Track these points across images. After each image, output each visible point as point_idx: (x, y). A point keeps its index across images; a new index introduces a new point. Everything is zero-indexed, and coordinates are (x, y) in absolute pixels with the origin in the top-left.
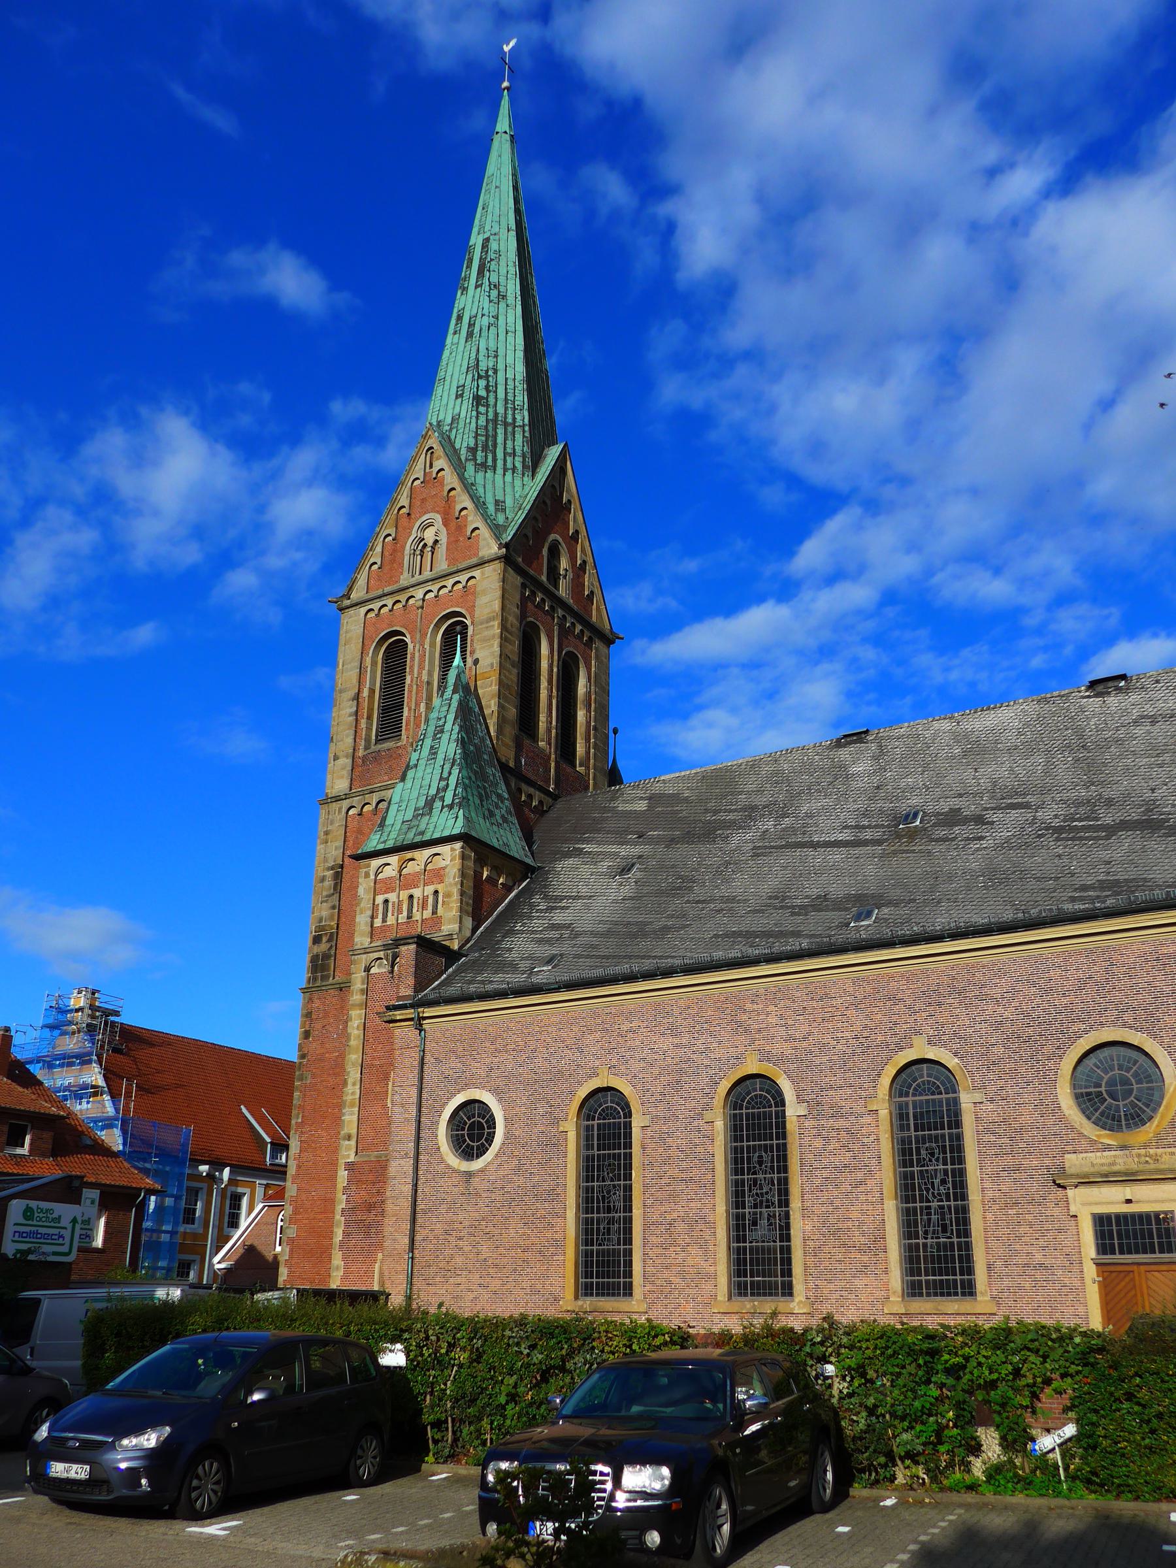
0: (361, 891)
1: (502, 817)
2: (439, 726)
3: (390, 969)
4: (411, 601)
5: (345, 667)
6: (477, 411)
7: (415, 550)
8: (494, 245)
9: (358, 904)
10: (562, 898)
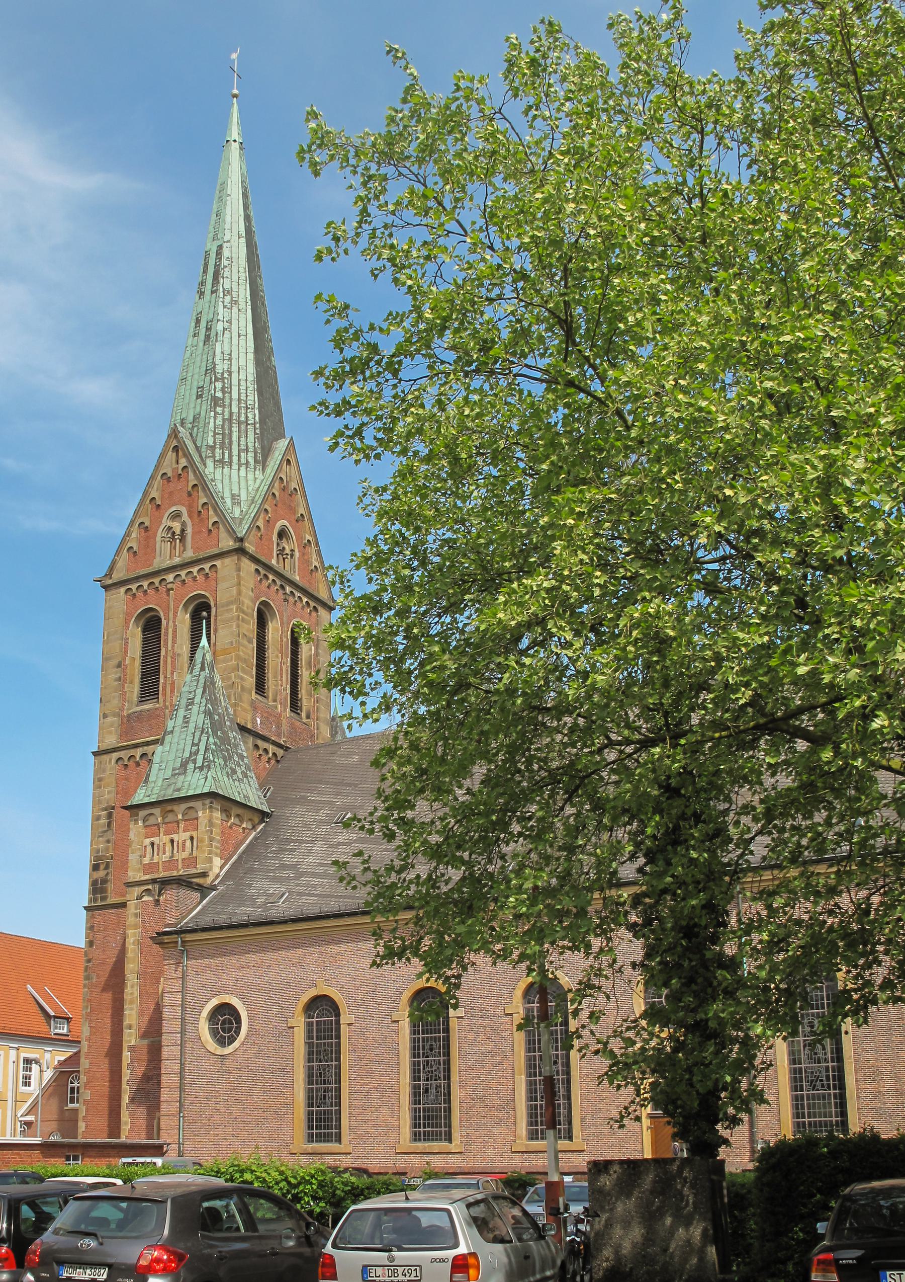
0: (132, 835)
8: (226, 253)
9: (129, 846)
10: (289, 841)
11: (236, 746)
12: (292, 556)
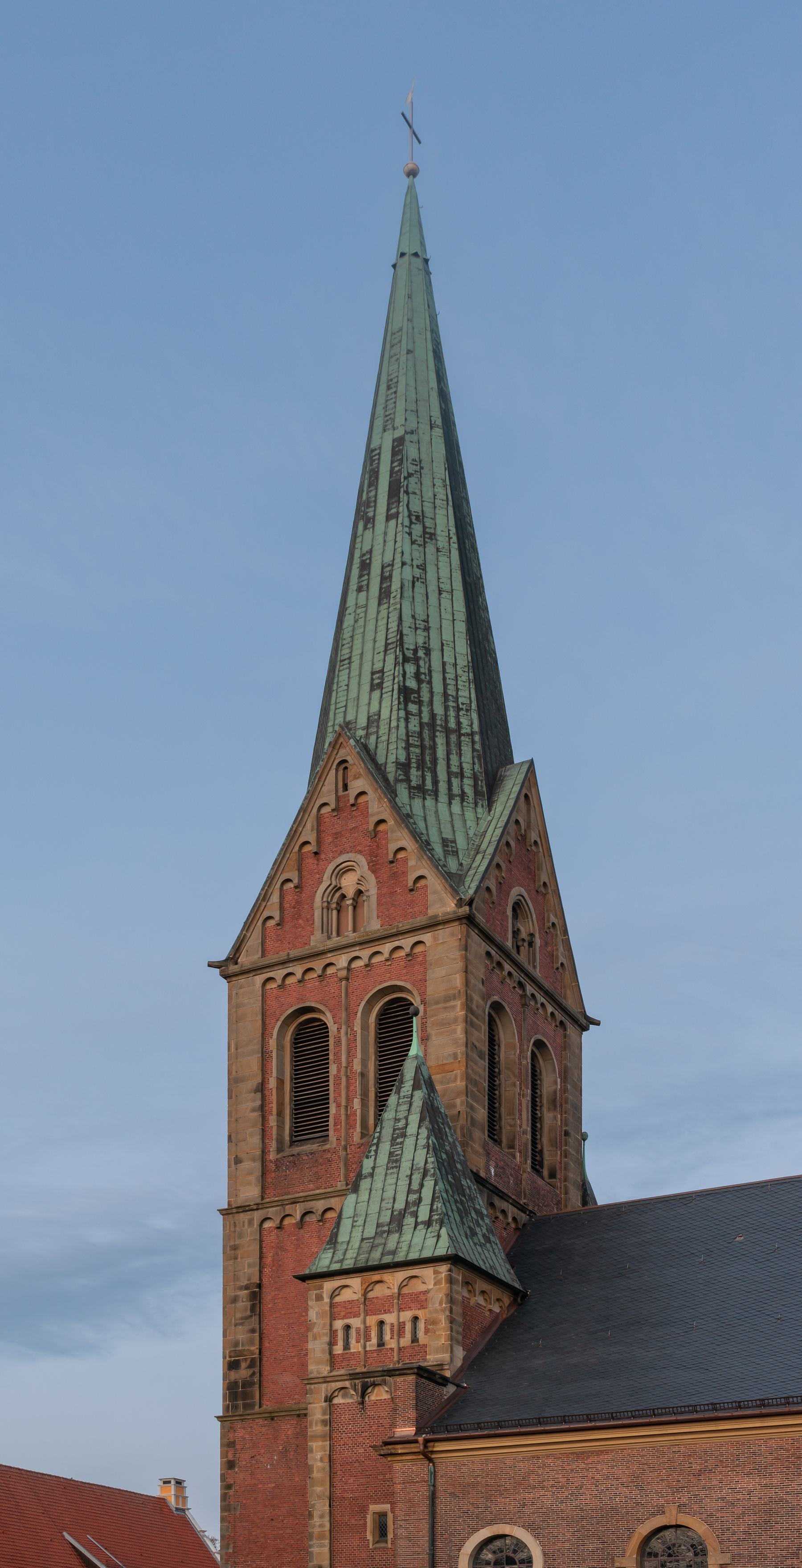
0: (312, 1315)
1: (484, 1236)
2: (398, 1129)
3: (360, 1399)
4: (330, 971)
5: (240, 1050)
6: (406, 710)
7: (328, 903)
8: (411, 451)
11: (472, 1199)
12: (531, 944)
